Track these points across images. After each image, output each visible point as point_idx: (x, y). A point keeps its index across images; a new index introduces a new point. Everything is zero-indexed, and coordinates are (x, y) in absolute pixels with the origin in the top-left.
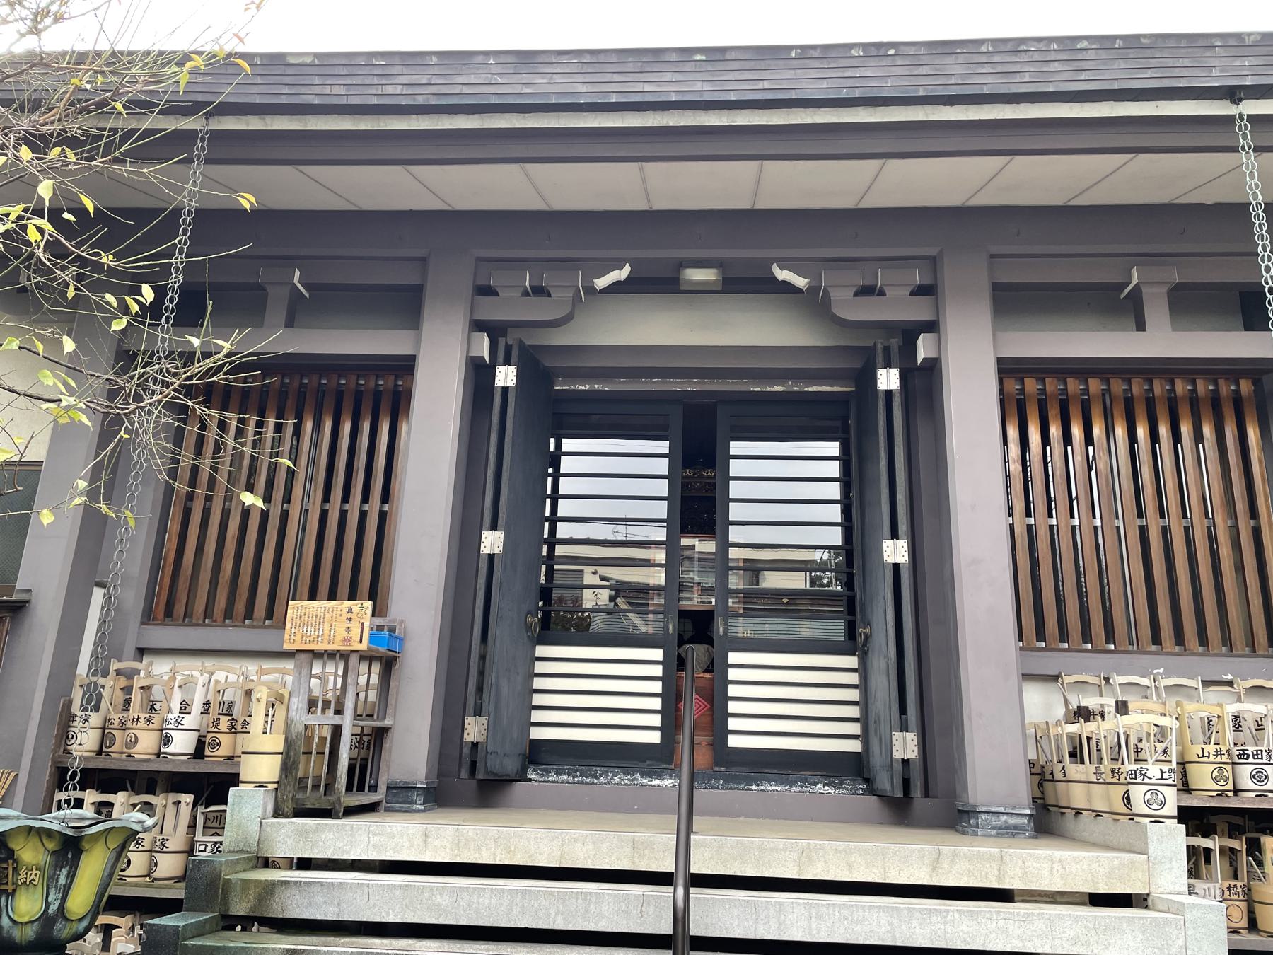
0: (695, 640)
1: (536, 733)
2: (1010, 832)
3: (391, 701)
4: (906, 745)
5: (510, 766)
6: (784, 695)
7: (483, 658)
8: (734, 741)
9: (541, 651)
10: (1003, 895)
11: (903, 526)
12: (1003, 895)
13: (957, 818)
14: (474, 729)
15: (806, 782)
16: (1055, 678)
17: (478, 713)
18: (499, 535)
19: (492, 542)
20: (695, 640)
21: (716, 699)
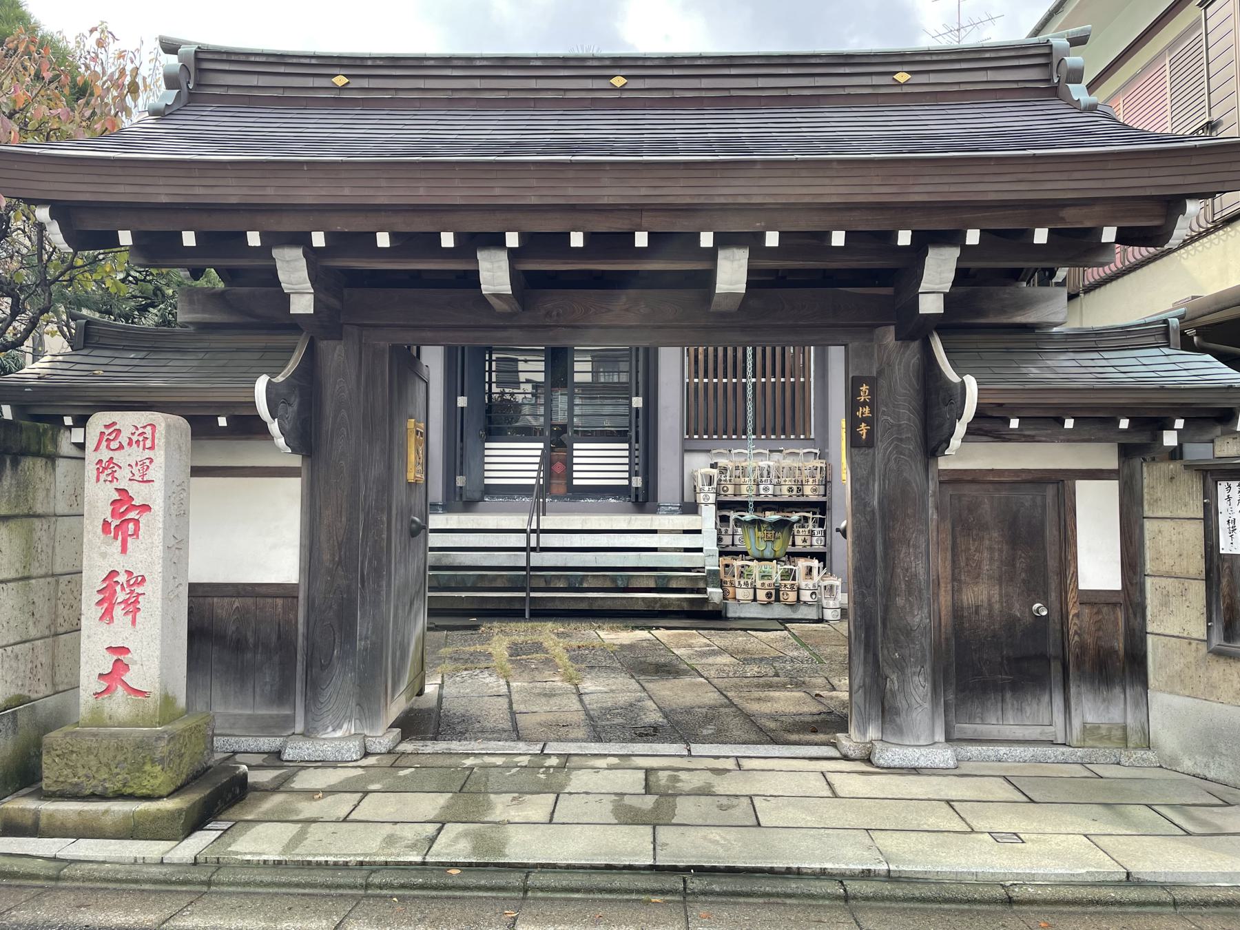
0: (558, 443)
1: (487, 481)
2: (672, 512)
3: (1190, 880)
4: (637, 482)
5: (477, 495)
6: (598, 462)
7: (462, 449)
8: (576, 482)
9: (487, 445)
10: (655, 532)
11: (641, 392)
12: (655, 532)
13: (655, 511)
14: (460, 481)
15: (605, 498)
16: (709, 451)
17: (461, 474)
18: (465, 398)
19: (462, 402)
20: (558, 443)
21: (568, 464)
